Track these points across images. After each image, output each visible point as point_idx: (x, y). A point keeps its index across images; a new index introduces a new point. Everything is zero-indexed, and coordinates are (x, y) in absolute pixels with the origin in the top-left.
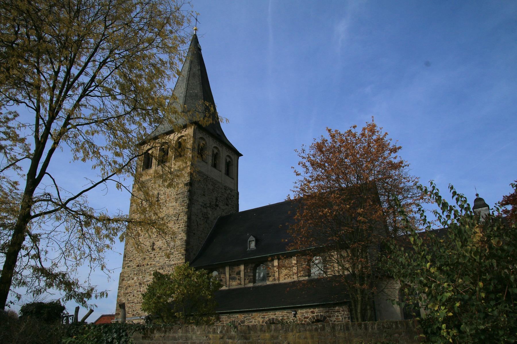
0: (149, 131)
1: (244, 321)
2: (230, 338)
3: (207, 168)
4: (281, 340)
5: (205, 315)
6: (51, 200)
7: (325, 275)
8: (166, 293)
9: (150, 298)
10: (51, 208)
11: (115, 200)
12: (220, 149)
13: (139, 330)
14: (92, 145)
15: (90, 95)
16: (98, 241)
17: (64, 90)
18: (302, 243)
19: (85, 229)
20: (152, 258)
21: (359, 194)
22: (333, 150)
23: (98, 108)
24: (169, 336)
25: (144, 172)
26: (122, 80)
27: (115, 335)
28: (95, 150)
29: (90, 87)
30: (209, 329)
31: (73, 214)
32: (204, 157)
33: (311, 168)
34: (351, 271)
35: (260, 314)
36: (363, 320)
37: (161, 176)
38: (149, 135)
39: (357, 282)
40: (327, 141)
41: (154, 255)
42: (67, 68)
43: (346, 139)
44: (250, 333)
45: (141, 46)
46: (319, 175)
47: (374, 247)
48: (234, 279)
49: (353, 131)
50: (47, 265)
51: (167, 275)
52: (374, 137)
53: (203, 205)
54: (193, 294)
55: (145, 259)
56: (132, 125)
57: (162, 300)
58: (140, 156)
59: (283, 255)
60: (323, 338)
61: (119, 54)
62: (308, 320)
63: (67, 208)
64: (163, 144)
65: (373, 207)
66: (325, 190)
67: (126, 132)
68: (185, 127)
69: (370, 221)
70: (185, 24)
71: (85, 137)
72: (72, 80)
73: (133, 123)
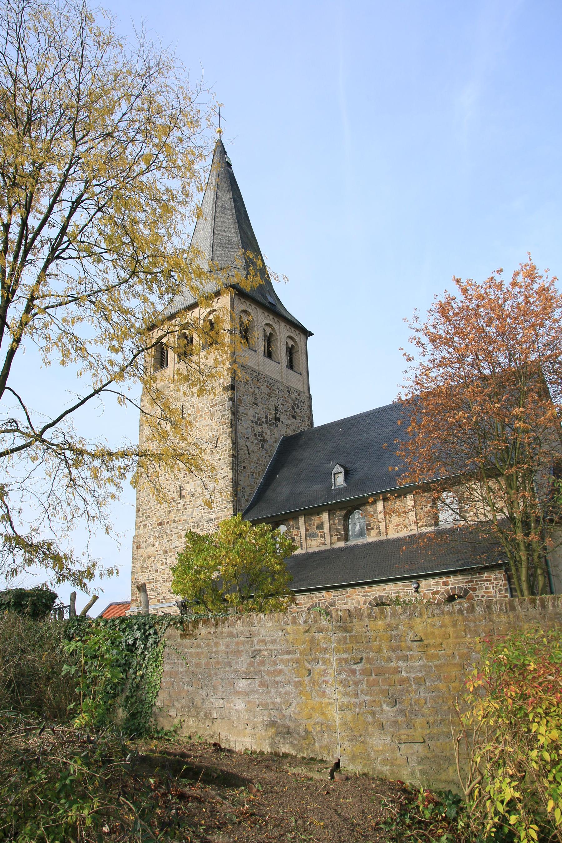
0: (159, 307)
1: (335, 602)
2: (321, 631)
3: (256, 360)
4: (404, 631)
5: (272, 595)
6: (18, 430)
7: (462, 523)
8: (207, 564)
9: (184, 573)
10: (20, 441)
11: (115, 422)
12: (276, 326)
13: (174, 624)
14: (74, 337)
15: (61, 258)
16: (96, 488)
17: (21, 254)
18: (422, 472)
19: (74, 471)
20: (180, 510)
21: (515, 385)
22: (466, 314)
23: (77, 278)
24: (222, 633)
25: (158, 374)
26: (108, 230)
27: (138, 634)
28: (79, 345)
29: (59, 244)
30: (286, 619)
31: (54, 450)
32: (251, 341)
33: (430, 347)
34: (507, 513)
35: (360, 590)
36: (532, 593)
37: (186, 379)
38: (159, 313)
39: (518, 530)
40: (454, 299)
41: (184, 505)
42: (22, 219)
43: (486, 293)
44: (351, 622)
45: (137, 169)
46: (444, 358)
47: (544, 472)
48: (312, 537)
49: (498, 278)
50: (23, 532)
51: (207, 536)
52: (536, 287)
53: (255, 420)
54: (251, 563)
55: (169, 512)
56: (132, 300)
57: (202, 576)
58: (149, 348)
59: (392, 492)
60: (472, 624)
61: (100, 185)
62: (438, 596)
63: (43, 441)
64: (184, 326)
65: (540, 404)
66: (457, 380)
67: (124, 311)
68: (218, 294)
69: (536, 428)
70: (204, 123)
71: (61, 327)
72: (31, 236)
73: (134, 296)
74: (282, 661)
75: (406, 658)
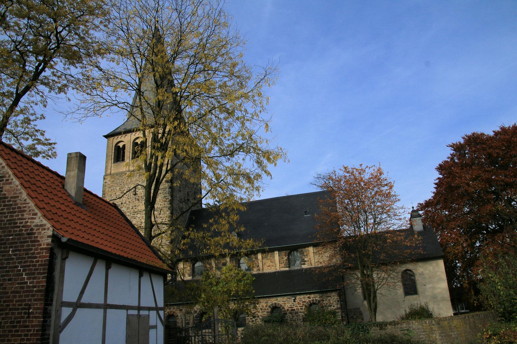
2: (433, 325)
74: (422, 335)
75: (453, 332)
